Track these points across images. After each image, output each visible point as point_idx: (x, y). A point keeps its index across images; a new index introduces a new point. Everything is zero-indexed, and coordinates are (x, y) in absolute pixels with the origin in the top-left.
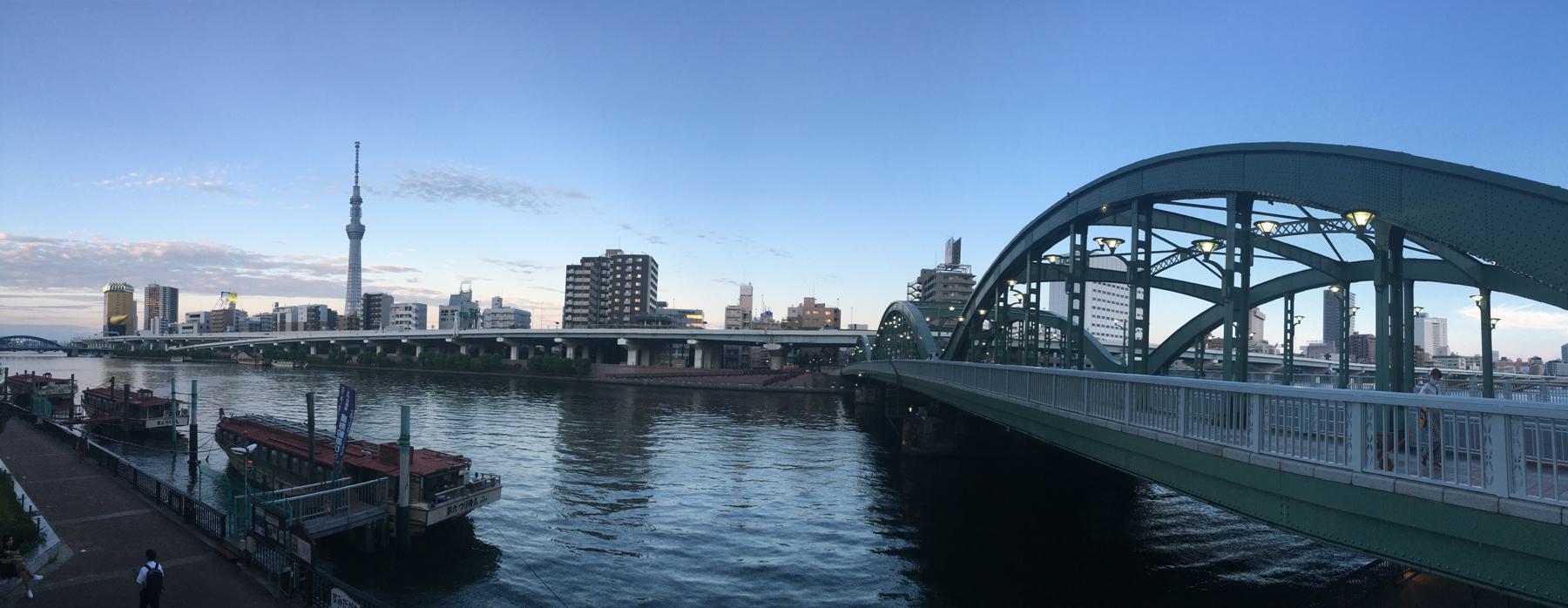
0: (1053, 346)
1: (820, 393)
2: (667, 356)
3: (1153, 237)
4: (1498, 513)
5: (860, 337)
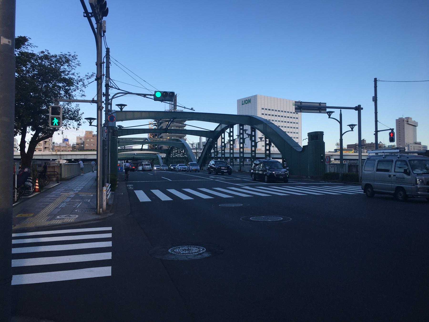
0: (235, 156)
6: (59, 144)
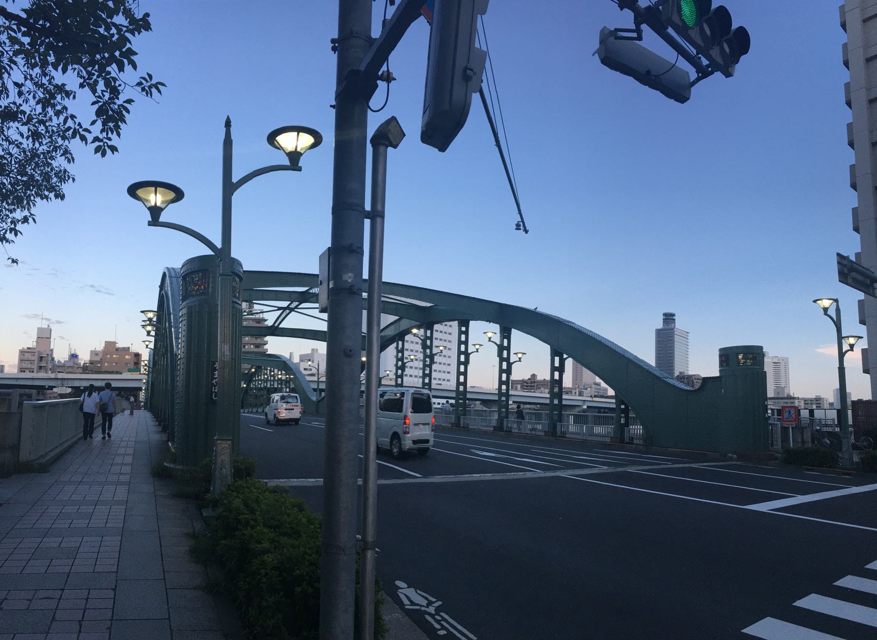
6: (63, 362)
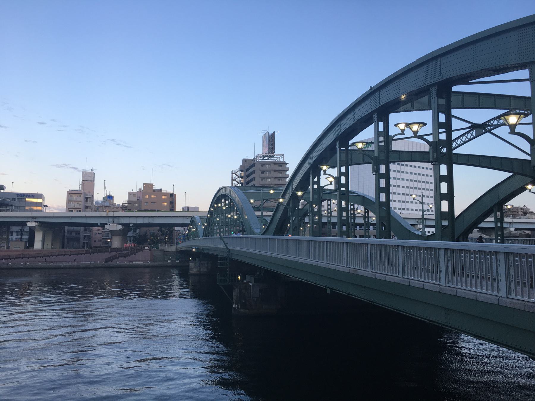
1: (156, 267)
2: (4, 239)
3: (453, 119)
4: (456, 295)
5: (192, 217)
